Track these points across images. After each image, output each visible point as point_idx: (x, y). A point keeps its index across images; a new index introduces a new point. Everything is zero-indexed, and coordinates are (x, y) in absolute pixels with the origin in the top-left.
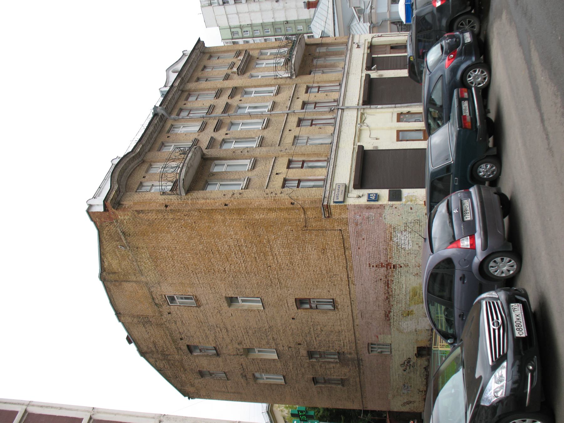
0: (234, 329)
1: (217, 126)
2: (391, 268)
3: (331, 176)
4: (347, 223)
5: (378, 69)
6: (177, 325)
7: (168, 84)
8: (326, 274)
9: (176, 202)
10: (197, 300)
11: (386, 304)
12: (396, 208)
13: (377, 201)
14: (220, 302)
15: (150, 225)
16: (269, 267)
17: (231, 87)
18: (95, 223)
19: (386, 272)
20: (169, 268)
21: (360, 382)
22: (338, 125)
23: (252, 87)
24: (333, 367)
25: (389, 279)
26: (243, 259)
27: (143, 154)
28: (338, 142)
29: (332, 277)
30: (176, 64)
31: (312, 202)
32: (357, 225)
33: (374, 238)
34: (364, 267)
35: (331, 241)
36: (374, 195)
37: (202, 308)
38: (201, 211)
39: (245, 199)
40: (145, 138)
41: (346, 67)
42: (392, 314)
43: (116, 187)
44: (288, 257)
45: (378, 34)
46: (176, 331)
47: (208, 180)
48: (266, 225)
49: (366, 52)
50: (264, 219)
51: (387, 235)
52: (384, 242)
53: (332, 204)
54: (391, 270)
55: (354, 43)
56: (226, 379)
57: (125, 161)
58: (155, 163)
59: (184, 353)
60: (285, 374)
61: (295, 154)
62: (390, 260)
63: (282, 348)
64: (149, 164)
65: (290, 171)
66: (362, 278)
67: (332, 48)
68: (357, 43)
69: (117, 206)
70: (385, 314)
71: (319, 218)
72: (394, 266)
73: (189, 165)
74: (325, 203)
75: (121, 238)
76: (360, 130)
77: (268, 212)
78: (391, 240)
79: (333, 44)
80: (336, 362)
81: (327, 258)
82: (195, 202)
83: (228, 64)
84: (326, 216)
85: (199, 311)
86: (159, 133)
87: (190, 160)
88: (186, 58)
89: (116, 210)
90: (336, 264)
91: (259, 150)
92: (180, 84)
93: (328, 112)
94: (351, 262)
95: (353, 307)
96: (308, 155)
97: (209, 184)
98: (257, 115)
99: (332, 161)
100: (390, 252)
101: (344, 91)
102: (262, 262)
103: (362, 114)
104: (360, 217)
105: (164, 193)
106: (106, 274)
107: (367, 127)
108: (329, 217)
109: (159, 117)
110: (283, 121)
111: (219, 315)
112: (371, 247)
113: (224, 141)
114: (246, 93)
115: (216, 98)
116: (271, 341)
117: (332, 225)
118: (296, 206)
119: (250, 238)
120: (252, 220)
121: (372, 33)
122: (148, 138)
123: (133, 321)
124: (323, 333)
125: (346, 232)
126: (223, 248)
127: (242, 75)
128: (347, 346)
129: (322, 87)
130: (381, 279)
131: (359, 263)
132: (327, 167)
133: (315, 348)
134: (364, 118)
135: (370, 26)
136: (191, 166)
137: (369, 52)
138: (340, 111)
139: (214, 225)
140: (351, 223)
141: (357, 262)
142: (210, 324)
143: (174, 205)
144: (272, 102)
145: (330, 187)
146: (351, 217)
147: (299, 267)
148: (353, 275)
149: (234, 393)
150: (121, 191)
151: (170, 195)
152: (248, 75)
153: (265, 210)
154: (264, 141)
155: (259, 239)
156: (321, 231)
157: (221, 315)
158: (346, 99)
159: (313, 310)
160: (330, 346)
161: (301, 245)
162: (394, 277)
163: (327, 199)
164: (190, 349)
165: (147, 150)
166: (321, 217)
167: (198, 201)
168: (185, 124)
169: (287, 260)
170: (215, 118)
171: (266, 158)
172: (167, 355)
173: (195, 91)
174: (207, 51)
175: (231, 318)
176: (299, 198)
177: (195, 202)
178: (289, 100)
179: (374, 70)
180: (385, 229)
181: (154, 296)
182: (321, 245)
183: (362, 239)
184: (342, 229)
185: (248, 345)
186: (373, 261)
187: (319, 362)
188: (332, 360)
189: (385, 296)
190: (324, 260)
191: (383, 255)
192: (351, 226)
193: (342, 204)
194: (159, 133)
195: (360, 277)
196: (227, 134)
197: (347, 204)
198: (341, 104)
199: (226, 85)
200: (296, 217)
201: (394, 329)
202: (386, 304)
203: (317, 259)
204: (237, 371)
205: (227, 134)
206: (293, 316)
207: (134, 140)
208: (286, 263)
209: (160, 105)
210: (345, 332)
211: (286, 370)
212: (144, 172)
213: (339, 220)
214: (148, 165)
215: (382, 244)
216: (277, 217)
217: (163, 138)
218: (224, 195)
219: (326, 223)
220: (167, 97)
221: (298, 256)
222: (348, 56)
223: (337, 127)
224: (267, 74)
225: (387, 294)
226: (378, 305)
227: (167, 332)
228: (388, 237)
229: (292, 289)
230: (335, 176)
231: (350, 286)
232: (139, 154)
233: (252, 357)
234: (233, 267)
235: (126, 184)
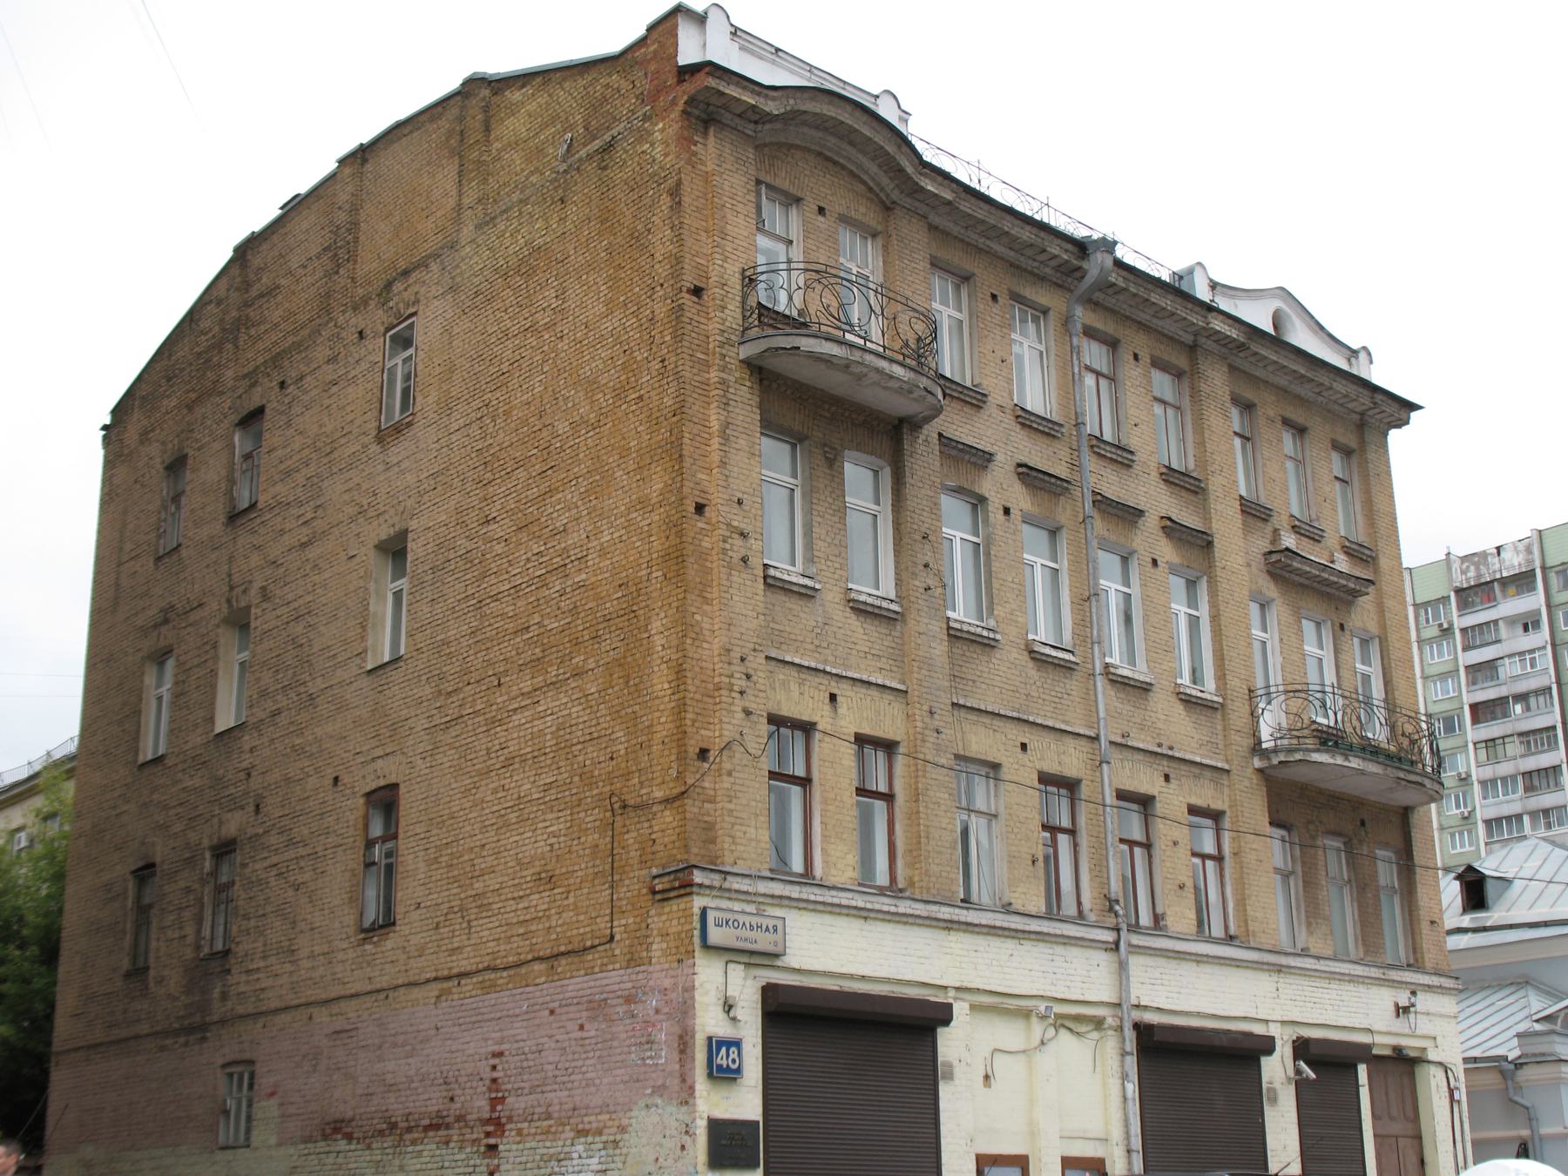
0: (308, 567)
1: (1041, 476)
2: (488, 1134)
3: (820, 899)
4: (633, 964)
5: (1301, 1085)
6: (325, 368)
7: (1224, 295)
8: (474, 893)
9: (713, 327)
10: (399, 429)
11: (375, 1121)
12: (683, 1147)
13: (710, 1075)
14: (392, 511)
15: (634, 236)
16: (496, 683)
17: (1210, 528)
18: (641, 42)
19: (474, 1116)
20: (499, 321)
21: (137, 1037)
22: (1045, 930)
23: (1214, 605)
24: (185, 936)
25: (451, 1132)
26: (524, 586)
27: (917, 204)
28: (971, 928)
29: (463, 917)
30: (1313, 324)
31: (710, 827)
32: (629, 1000)
33: (584, 1069)
34: (494, 1035)
35: (576, 907)
36: (734, 1061)
37: (375, 448)
38: (675, 419)
39: (724, 576)
40: (981, 212)
41: (1308, 963)
42: (342, 1145)
43: (772, 107)
44: (529, 749)
45: (1464, 1090)
46: (308, 365)
47: (806, 443)
48: (629, 659)
49: (1379, 1039)
50: (649, 652)
51: (592, 1118)
52: (570, 1106)
53: (698, 902)
54: (482, 1136)
55: (1414, 993)
56: (161, 553)
57: (880, 138)
58: (880, 252)
59: (240, 397)
60: (169, 762)
61: (916, 765)
62: (514, 1133)
63: (247, 747)
64: (879, 228)
65: (848, 752)
66: (456, 1029)
67: (1392, 912)
68: (1413, 1005)
69: (696, 112)
70: (343, 1121)
71: (651, 856)
72: (493, 1148)
73: (856, 369)
74: (698, 877)
75: (595, 138)
76: (1026, 1014)
77: (670, 664)
78: (578, 1132)
79: (1411, 915)
80: (198, 947)
81: (521, 893)
82: (712, 394)
83: (1314, 516)
84: (657, 881)
85: (366, 440)
86: (1012, 265)
87: (878, 371)
88: (1341, 364)
89: (684, 112)
90: (505, 928)
91: (937, 628)
92: (1221, 336)
93: (1106, 891)
94: (510, 986)
95: (367, 998)
96: (913, 816)
97: (794, 446)
98: (1091, 622)
99: (885, 904)
100: (539, 1131)
101: (1196, 955)
102: (514, 653)
103: (1098, 1023)
104: (651, 1012)
105: (749, 281)
106: (483, 99)
107: (1037, 1042)
108: (654, 892)
109: (1075, 262)
110: (1066, 722)
111: (351, 510)
112: (557, 1059)
113: (978, 502)
114: (1191, 584)
115: (1164, 470)
116: (270, 706)
117: (629, 907)
118: (692, 769)
119: (590, 605)
120: (647, 606)
121: (1466, 1070)
122: (983, 222)
123: (340, 208)
124: (290, 893)
125: (605, 960)
126: (558, 507)
127: (1265, 569)
128: (247, 982)
129: (1222, 870)
130: (452, 1099)
131: (505, 1013)
132: (780, 871)
133: (244, 866)
134: (1082, 1028)
135: (1505, 1058)
136: (860, 378)
137: (1375, 1052)
138: (1109, 936)
139: (631, 468)
140: (633, 977)
141: (507, 1006)
142: (326, 483)
143: (702, 320)
144: (1148, 680)
145: (772, 896)
146: (655, 975)
147: (495, 791)
148: (468, 995)
149: (117, 585)
150: (760, 127)
151: (743, 302)
152: (1265, 590)
153: (680, 654)
154: (978, 649)
155: (587, 637)
156: (608, 867)
157: (352, 520)
158: (1161, 961)
159: (362, 852)
160: (249, 919)
161: (567, 793)
162: (460, 1148)
163: (717, 884)
164: (252, 419)
165: (935, 219)
166: (657, 862)
167: (716, 404)
168: (1052, 357)
169: (517, 747)
170: (1075, 466)
171: (900, 658)
172: (236, 338)
173: (1195, 395)
174: (1370, 436)
175: (343, 557)
176: (725, 778)
177: (712, 394)
178: (1160, 745)
179: (1298, 1072)
180: (612, 1108)
181: (414, 276)
182: (564, 870)
183: (583, 1021)
184: (614, 945)
185: (259, 622)
186: (512, 1066)
187: (203, 882)
188: (206, 932)
189: (399, 1119)
190: (516, 881)
191: (530, 1103)
192: (626, 978)
193: (697, 940)
194: (1012, 265)
195: (461, 1021)
196: (1007, 511)
197: (698, 961)
198: (1136, 940)
199: (1219, 508)
200: (654, 769)
201: (295, 1157)
202: (375, 1121)
203: (520, 856)
204: (183, 591)
205: (1007, 511)
206: (346, 779)
207: (983, 175)
208: (510, 743)
209: (1119, 264)
210: (291, 973)
211: (180, 767)
212: (842, 210)
213: (644, 932)
214: (873, 223)
215: (564, 1100)
216: (657, 698)
217: (989, 278)
218: (740, 502)
219: (633, 884)
220: (1159, 290)
221: (529, 786)
222: (1359, 970)
223: (1034, 926)
224: (1275, 661)
225: (405, 1124)
226: (370, 1091)
227: (305, 332)
228: (586, 1119)
229: (427, 771)
230: (819, 915)
231: (434, 985)
232: (916, 191)
233: (222, 641)
234: (499, 548)
235: (791, 146)
